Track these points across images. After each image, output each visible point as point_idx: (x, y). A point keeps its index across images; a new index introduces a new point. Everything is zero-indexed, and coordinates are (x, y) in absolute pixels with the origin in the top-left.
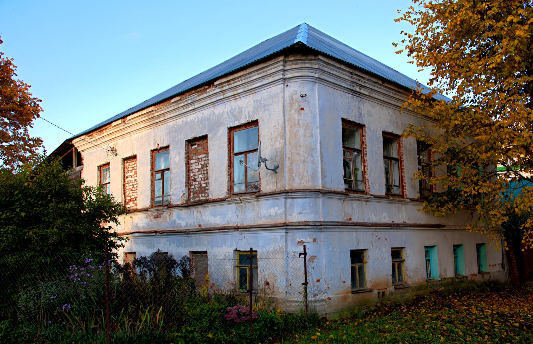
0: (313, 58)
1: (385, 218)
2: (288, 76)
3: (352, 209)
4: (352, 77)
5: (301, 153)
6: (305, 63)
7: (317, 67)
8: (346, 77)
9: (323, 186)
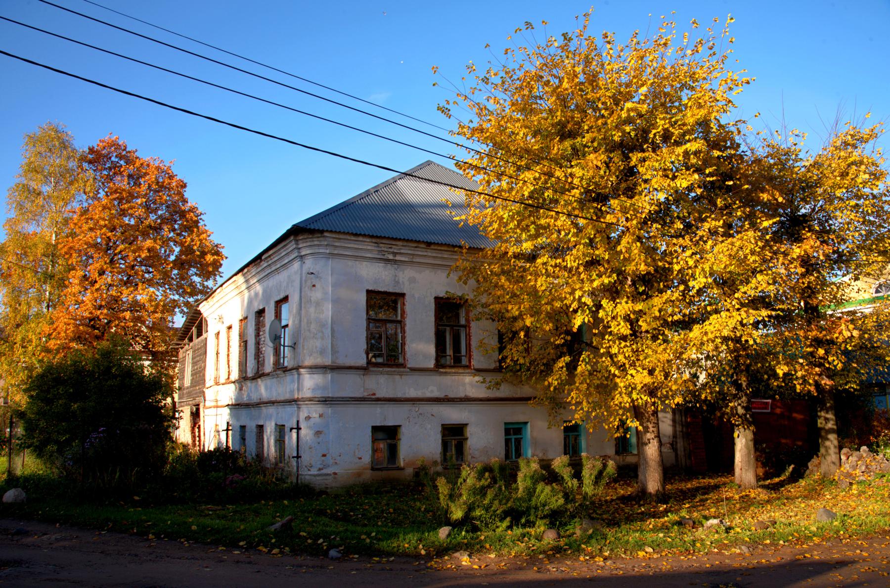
0: (319, 235)
1: (432, 391)
2: (303, 253)
4: (378, 247)
6: (313, 241)
7: (326, 243)
8: (369, 248)
9: (333, 362)
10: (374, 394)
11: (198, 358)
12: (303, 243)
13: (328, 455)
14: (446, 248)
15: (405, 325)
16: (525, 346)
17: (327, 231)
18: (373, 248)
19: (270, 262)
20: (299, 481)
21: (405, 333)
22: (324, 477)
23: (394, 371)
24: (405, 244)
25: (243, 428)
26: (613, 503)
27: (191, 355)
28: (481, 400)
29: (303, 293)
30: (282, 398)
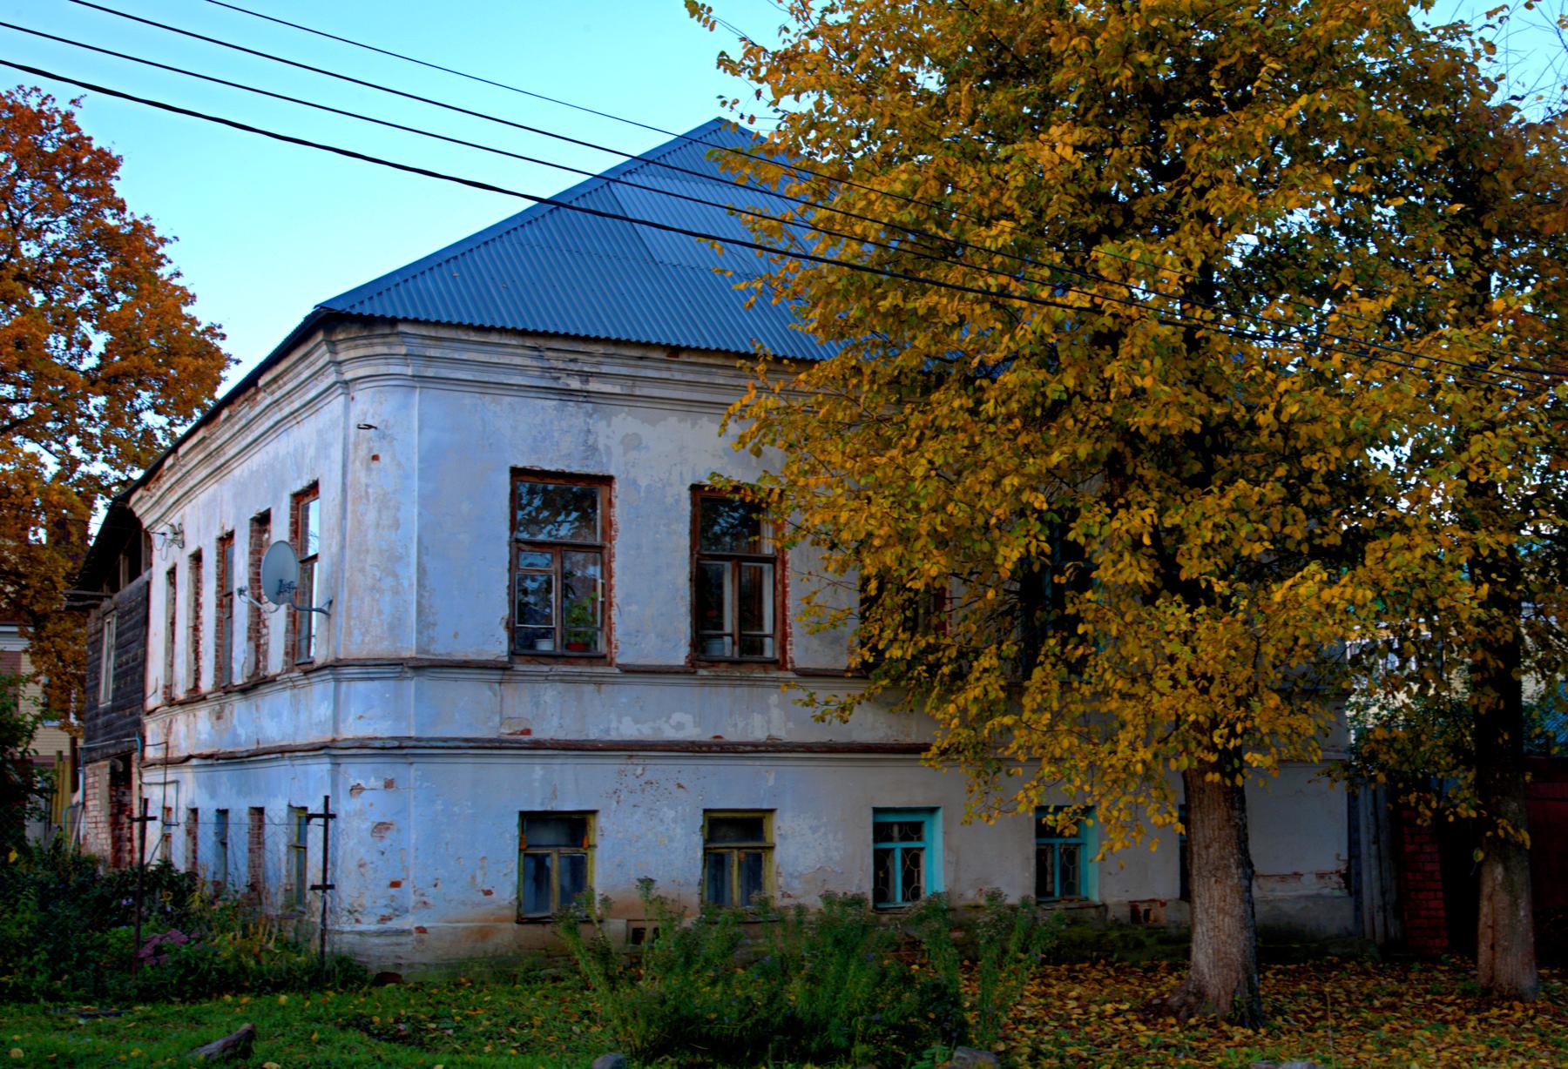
0: (387, 331)
1: (680, 726)
2: (348, 376)
3: (537, 704)
4: (541, 358)
5: (368, 568)
6: (372, 345)
7: (403, 350)
8: (517, 361)
9: (420, 650)
10: (527, 732)
11: (129, 635)
12: (348, 349)
13: (404, 884)
14: (719, 361)
15: (611, 556)
16: (908, 613)
17: (405, 320)
18: (528, 362)
19: (278, 395)
20: (327, 949)
21: (611, 577)
22: (394, 939)
23: (580, 674)
24: (612, 350)
25: (223, 813)
26: (1118, 1020)
27: (114, 626)
28: (808, 748)
29: (350, 477)
30: (301, 740)
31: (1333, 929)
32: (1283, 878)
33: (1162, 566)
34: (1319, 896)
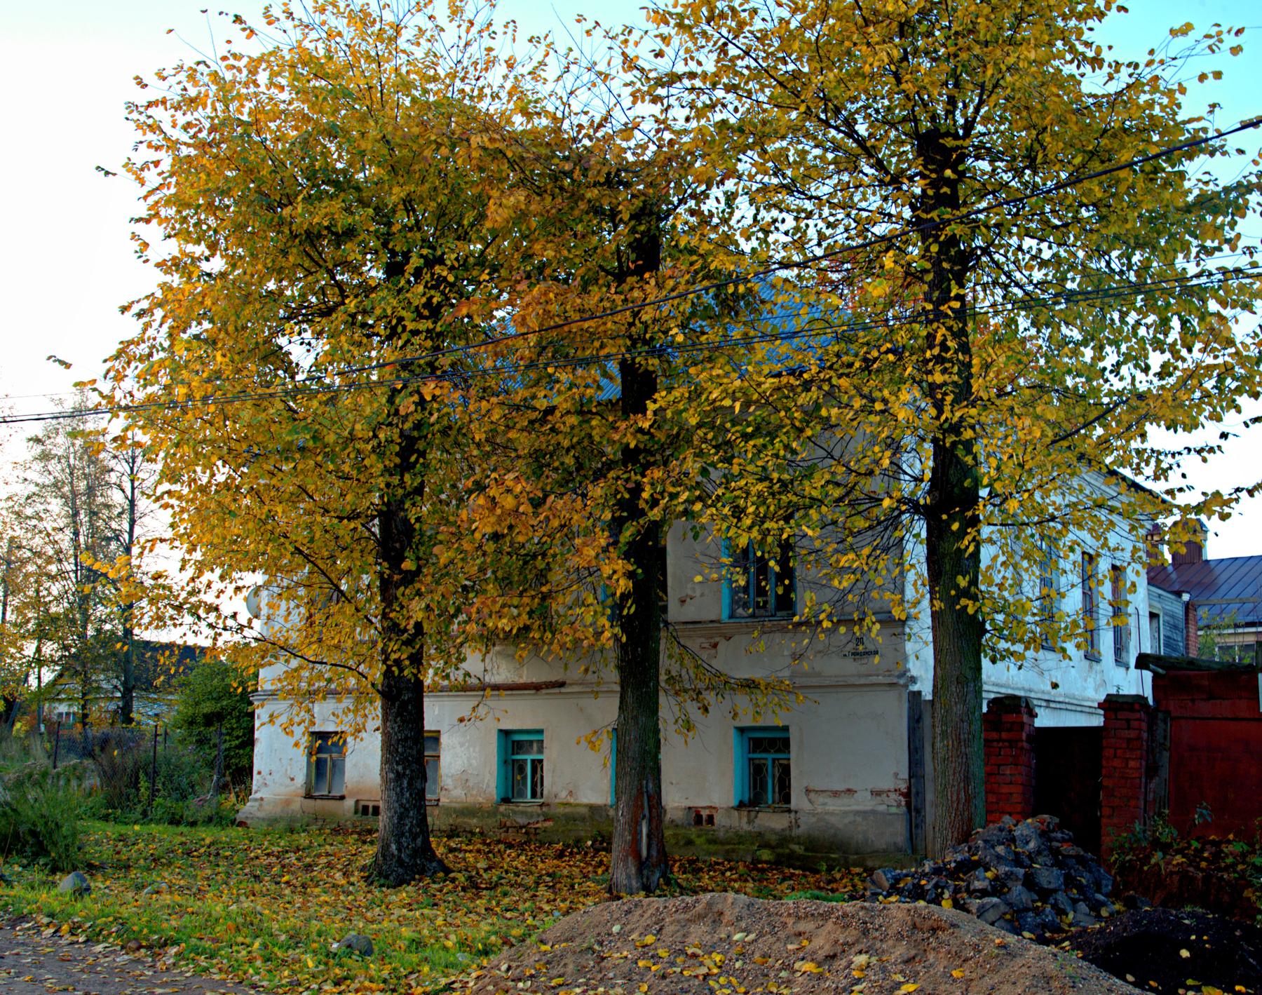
31: (881, 843)
32: (836, 794)
33: (639, 563)
34: (873, 812)
